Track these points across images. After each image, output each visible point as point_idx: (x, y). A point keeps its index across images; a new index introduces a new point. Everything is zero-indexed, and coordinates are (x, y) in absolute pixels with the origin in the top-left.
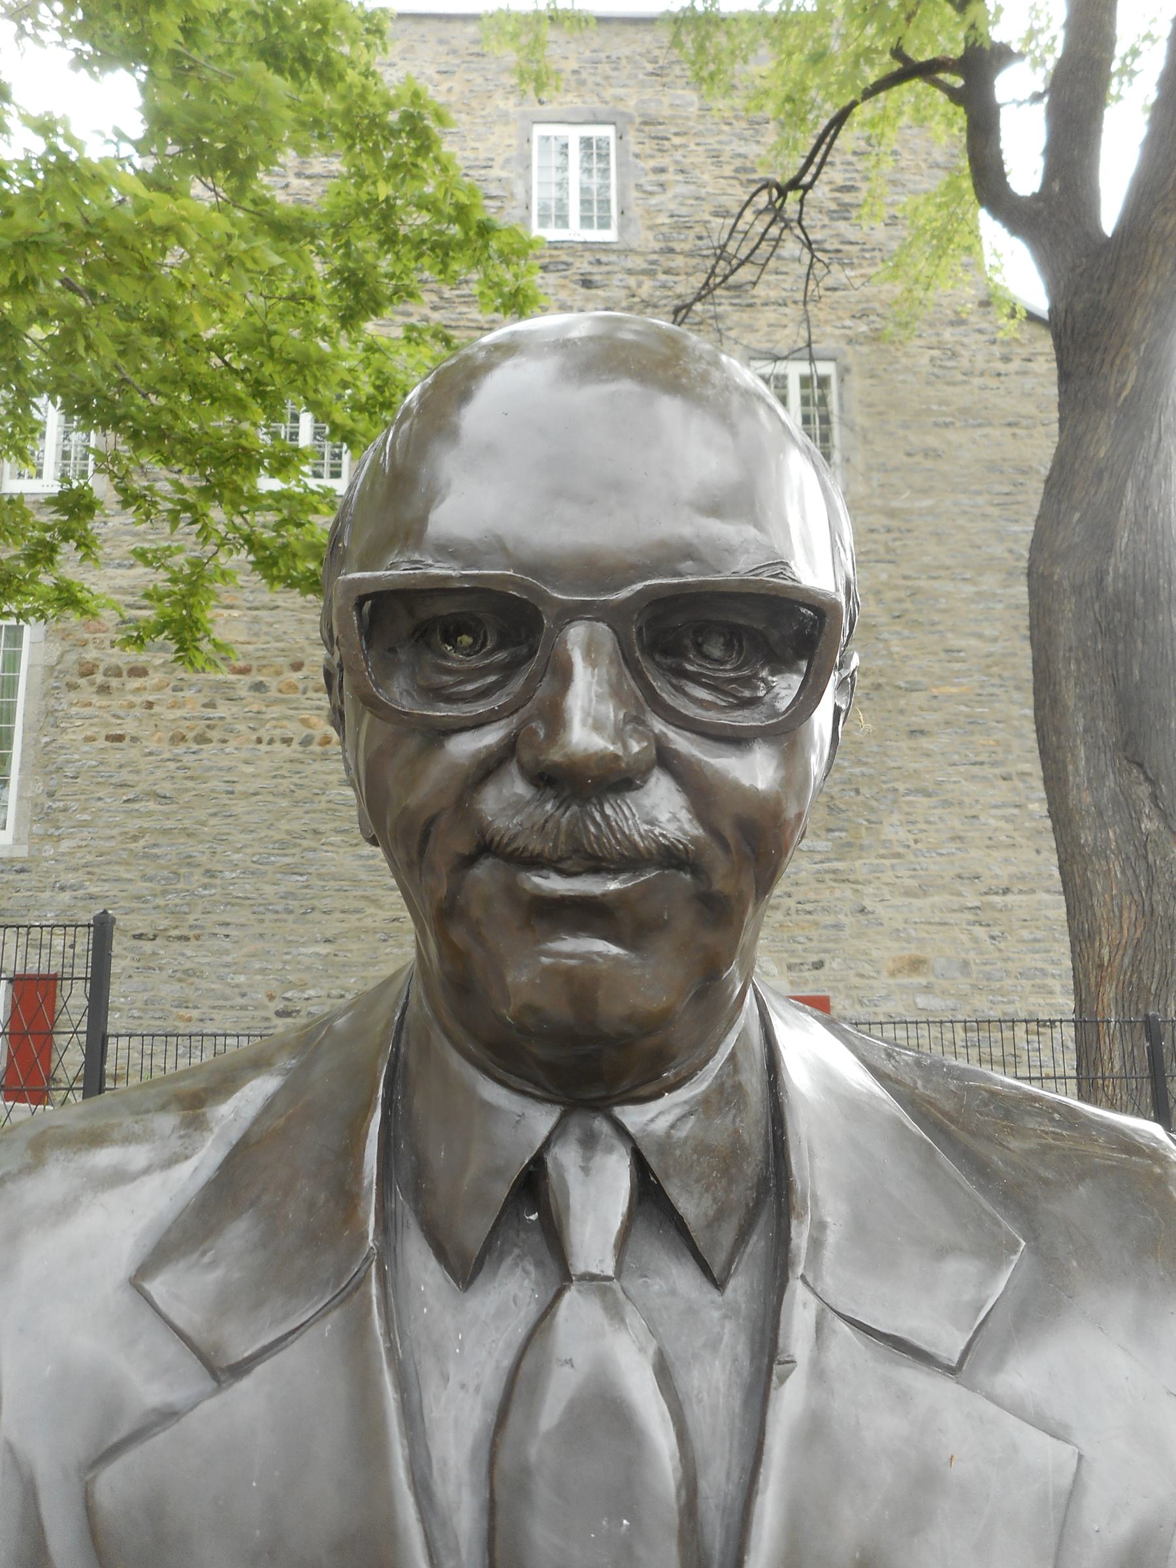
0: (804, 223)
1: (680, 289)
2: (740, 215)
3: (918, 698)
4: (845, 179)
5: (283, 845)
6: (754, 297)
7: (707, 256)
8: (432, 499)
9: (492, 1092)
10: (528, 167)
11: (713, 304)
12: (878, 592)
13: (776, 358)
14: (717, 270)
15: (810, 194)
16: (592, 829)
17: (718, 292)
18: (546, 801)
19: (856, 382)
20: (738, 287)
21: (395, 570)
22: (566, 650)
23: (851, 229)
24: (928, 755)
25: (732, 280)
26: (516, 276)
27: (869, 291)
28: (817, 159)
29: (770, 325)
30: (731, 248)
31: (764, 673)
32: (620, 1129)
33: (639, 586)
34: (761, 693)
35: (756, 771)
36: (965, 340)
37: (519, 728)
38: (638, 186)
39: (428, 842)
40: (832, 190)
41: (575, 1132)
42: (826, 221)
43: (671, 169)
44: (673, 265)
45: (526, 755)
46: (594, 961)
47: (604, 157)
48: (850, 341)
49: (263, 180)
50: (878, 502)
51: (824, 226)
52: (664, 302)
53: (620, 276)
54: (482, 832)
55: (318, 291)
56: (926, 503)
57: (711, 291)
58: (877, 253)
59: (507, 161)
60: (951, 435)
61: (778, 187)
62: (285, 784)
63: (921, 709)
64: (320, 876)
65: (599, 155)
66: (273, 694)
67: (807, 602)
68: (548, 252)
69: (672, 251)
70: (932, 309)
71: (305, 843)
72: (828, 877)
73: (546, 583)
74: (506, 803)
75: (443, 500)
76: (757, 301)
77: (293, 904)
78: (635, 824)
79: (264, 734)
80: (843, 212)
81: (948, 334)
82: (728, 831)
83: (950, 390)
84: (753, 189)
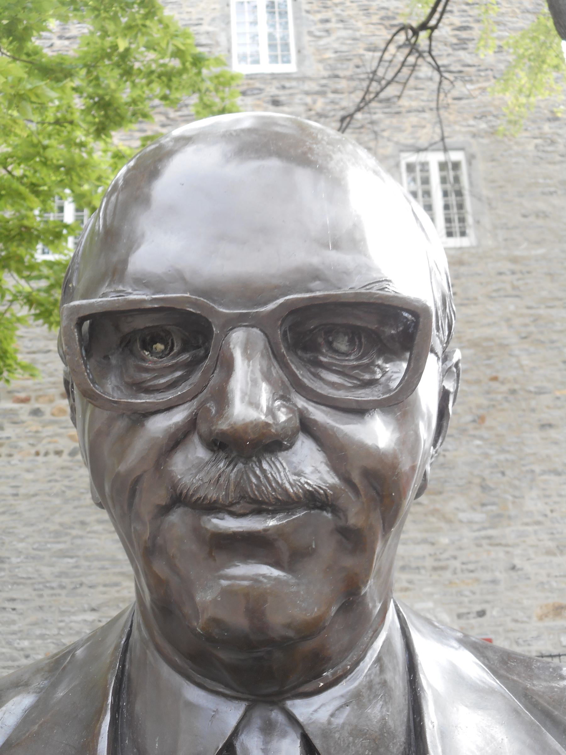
0: (434, 53)
1: (344, 104)
2: (385, 50)
3: (546, 399)
4: (462, 22)
5: (57, 534)
6: (400, 107)
7: (363, 80)
8: (132, 247)
9: (194, 694)
10: (228, 23)
11: (369, 113)
12: (508, 320)
13: (419, 150)
14: (371, 89)
15: (436, 33)
16: (254, 480)
17: (373, 104)
18: (220, 461)
19: (481, 166)
20: (388, 100)
21: (105, 298)
22: (229, 349)
23: (468, 56)
24: (556, 443)
25: (382, 95)
26: (223, 99)
27: (486, 98)
28: (440, 9)
29: (413, 127)
30: (380, 73)
31: (380, 362)
32: (292, 719)
33: (281, 301)
34: (378, 376)
35: (378, 433)
36: (560, 131)
37: (198, 409)
38: (310, 33)
39: (131, 494)
40: (454, 29)
41: (257, 722)
42: (450, 51)
43: (334, 20)
44: (339, 86)
45: (203, 428)
46: (261, 582)
47: (283, 14)
48: (474, 135)
49: (35, 42)
50: (504, 252)
51: (449, 55)
52: (332, 113)
53: (299, 96)
54: (174, 487)
55: (77, 116)
56: (541, 251)
57: (367, 104)
58: (489, 72)
59: (213, 20)
60: (555, 201)
61: (412, 28)
62: (58, 487)
63: (548, 407)
64: (87, 558)
65: (280, 13)
66: (47, 417)
67: (405, 307)
68: (246, 82)
69: (337, 76)
70: (533, 110)
71: (74, 532)
72: (484, 542)
73: (214, 301)
74: (192, 465)
75: (139, 247)
76: (403, 110)
77: (65, 581)
78: (286, 476)
79: (41, 448)
80: (462, 44)
81: (547, 128)
82: (356, 478)
83: (551, 167)
84: (394, 30)
